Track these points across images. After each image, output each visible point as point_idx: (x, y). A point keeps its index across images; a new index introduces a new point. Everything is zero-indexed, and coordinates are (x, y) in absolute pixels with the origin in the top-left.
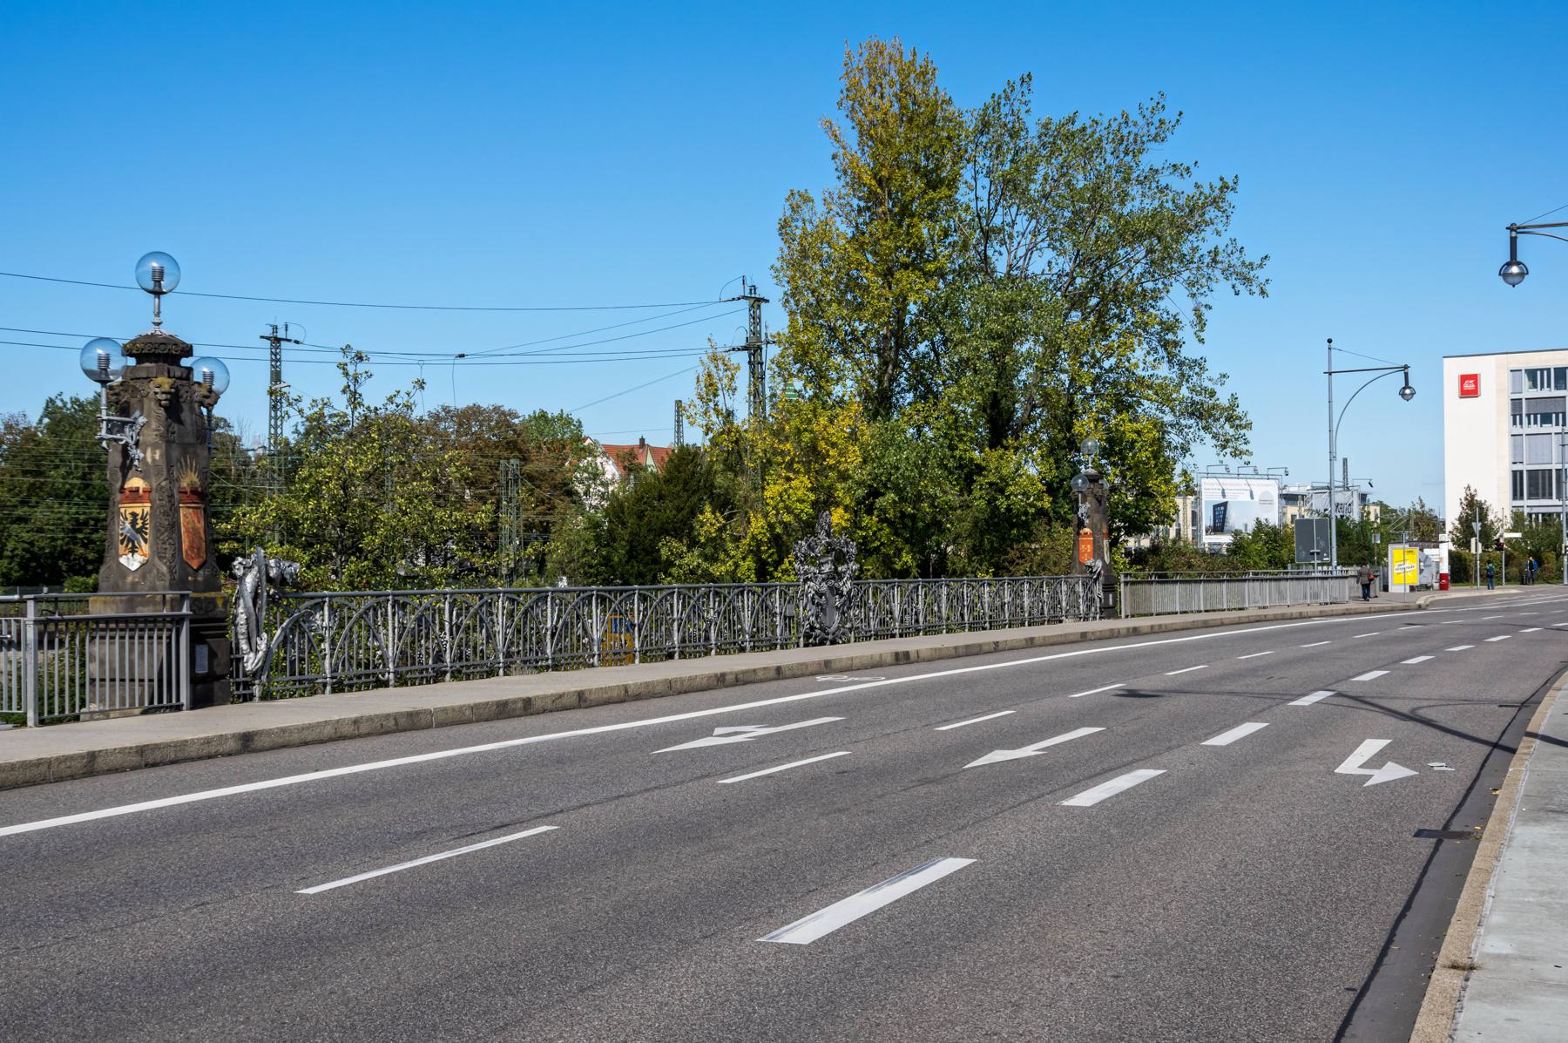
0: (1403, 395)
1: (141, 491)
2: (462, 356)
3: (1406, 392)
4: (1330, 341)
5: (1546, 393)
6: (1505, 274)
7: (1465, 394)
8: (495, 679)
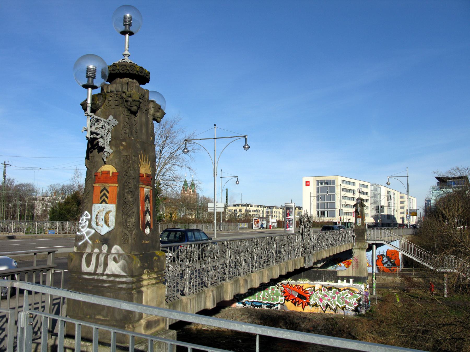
1: (111, 175)
2: (40, 169)
3: (237, 182)
4: (221, 170)
5: (323, 186)
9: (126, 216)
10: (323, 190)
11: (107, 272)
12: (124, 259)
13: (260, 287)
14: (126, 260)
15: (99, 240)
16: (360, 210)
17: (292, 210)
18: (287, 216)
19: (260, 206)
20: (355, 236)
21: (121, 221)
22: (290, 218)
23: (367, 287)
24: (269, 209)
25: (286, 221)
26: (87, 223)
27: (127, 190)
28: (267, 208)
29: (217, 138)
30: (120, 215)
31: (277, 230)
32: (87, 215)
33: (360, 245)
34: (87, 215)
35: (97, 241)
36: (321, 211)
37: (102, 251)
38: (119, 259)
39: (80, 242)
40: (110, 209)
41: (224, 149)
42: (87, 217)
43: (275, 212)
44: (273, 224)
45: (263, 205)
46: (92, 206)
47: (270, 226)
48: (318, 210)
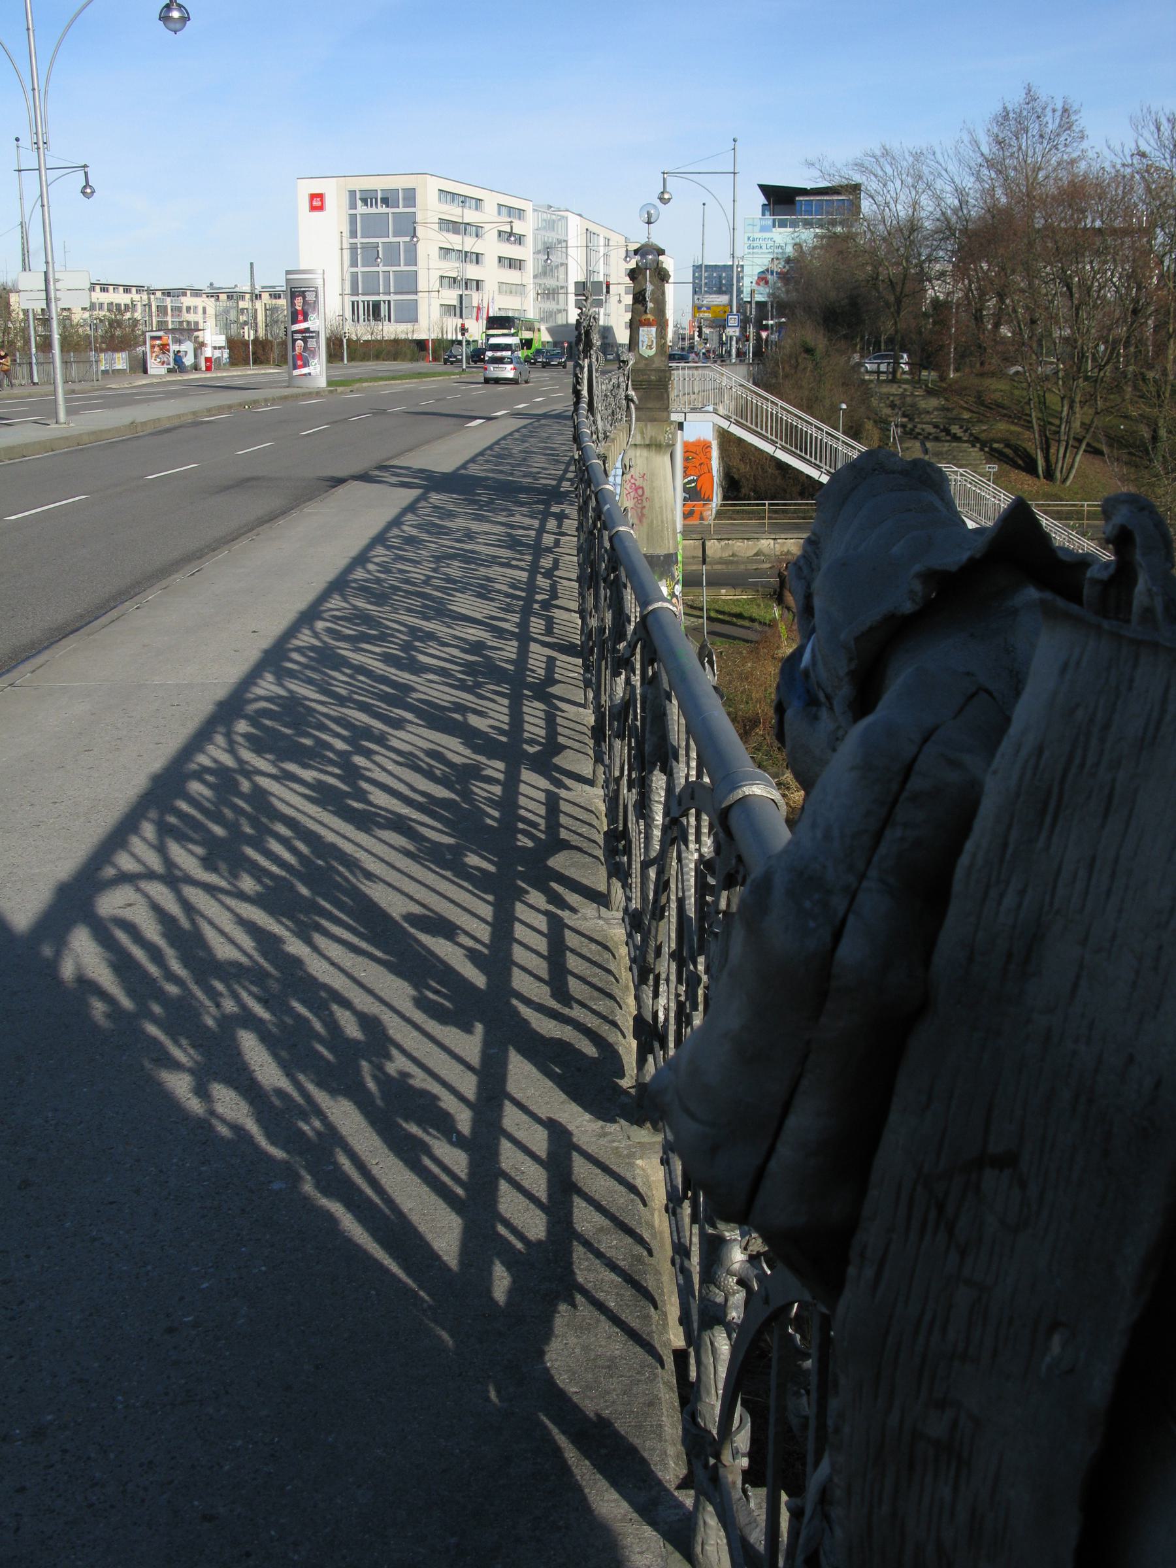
0: (83, 193)
3: (87, 191)
4: (17, 140)
5: (373, 210)
7: (313, 208)
8: (339, 364)
10: (373, 225)
16: (653, 292)
17: (317, 296)
18: (294, 321)
19: (134, 290)
20: (635, 398)
22: (307, 330)
23: (677, 593)
24: (169, 299)
25: (294, 341)
28: (159, 294)
33: (651, 430)
36: (368, 301)
41: (73, 21)
43: (188, 309)
44: (217, 354)
45: (146, 284)
47: (208, 360)
48: (355, 298)
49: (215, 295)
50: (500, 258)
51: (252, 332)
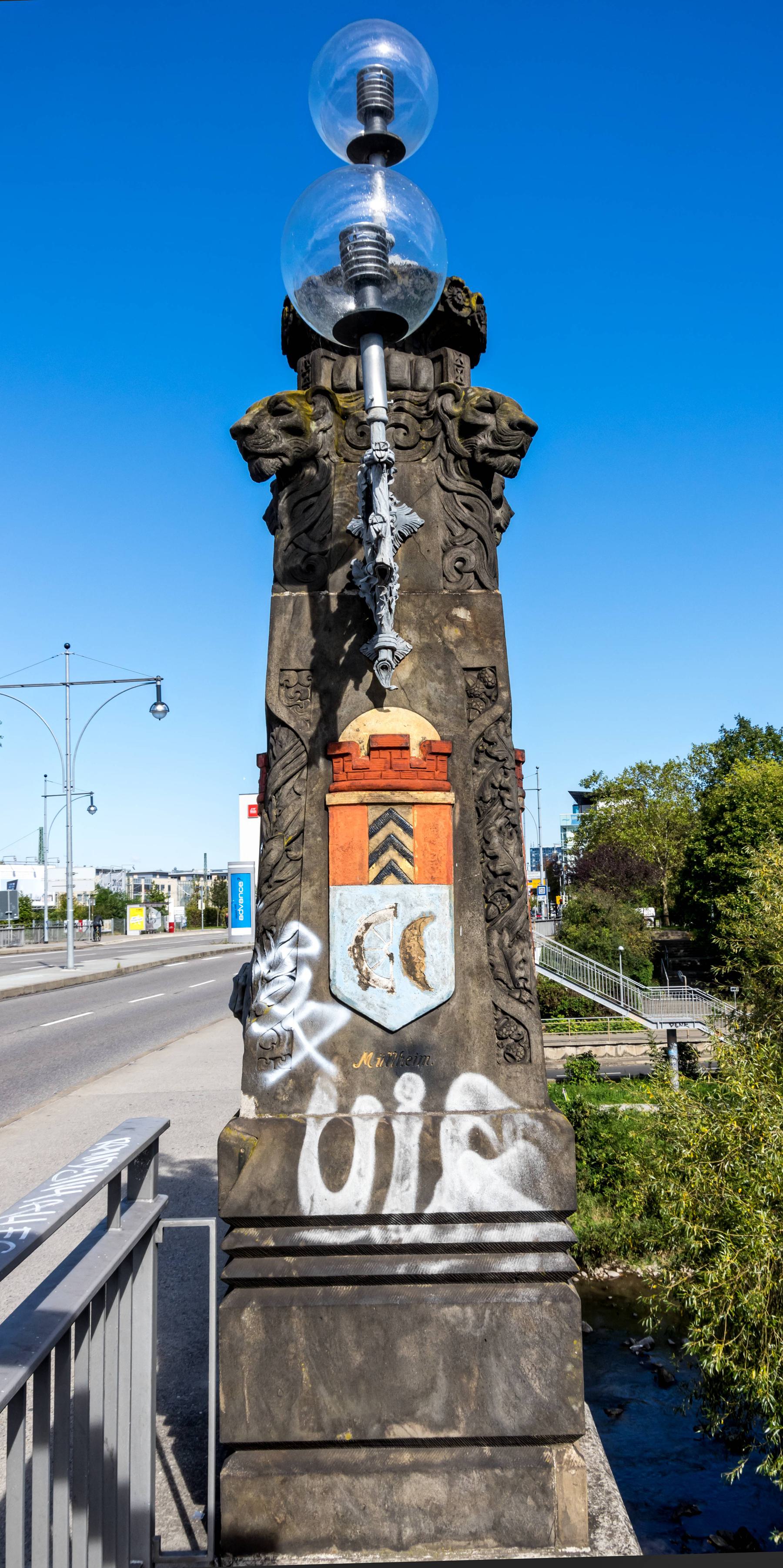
0: (89, 810)
1: (415, 752)
3: (92, 809)
4: (46, 776)
6: (153, 711)
9: (507, 939)
11: (439, 1204)
12: (525, 1137)
13: (341, 1115)
14: (536, 1143)
15: (377, 1055)
21: (486, 961)
26: (306, 975)
27: (500, 822)
29: (72, 684)
30: (478, 934)
31: (201, 933)
32: (298, 942)
34: (298, 942)
35: (366, 1058)
37: (397, 1104)
38: (501, 1140)
39: (267, 1068)
40: (426, 909)
42: (302, 951)
46: (323, 897)
49: (178, 877)
50: (530, 430)
51: (204, 904)
